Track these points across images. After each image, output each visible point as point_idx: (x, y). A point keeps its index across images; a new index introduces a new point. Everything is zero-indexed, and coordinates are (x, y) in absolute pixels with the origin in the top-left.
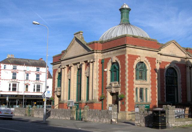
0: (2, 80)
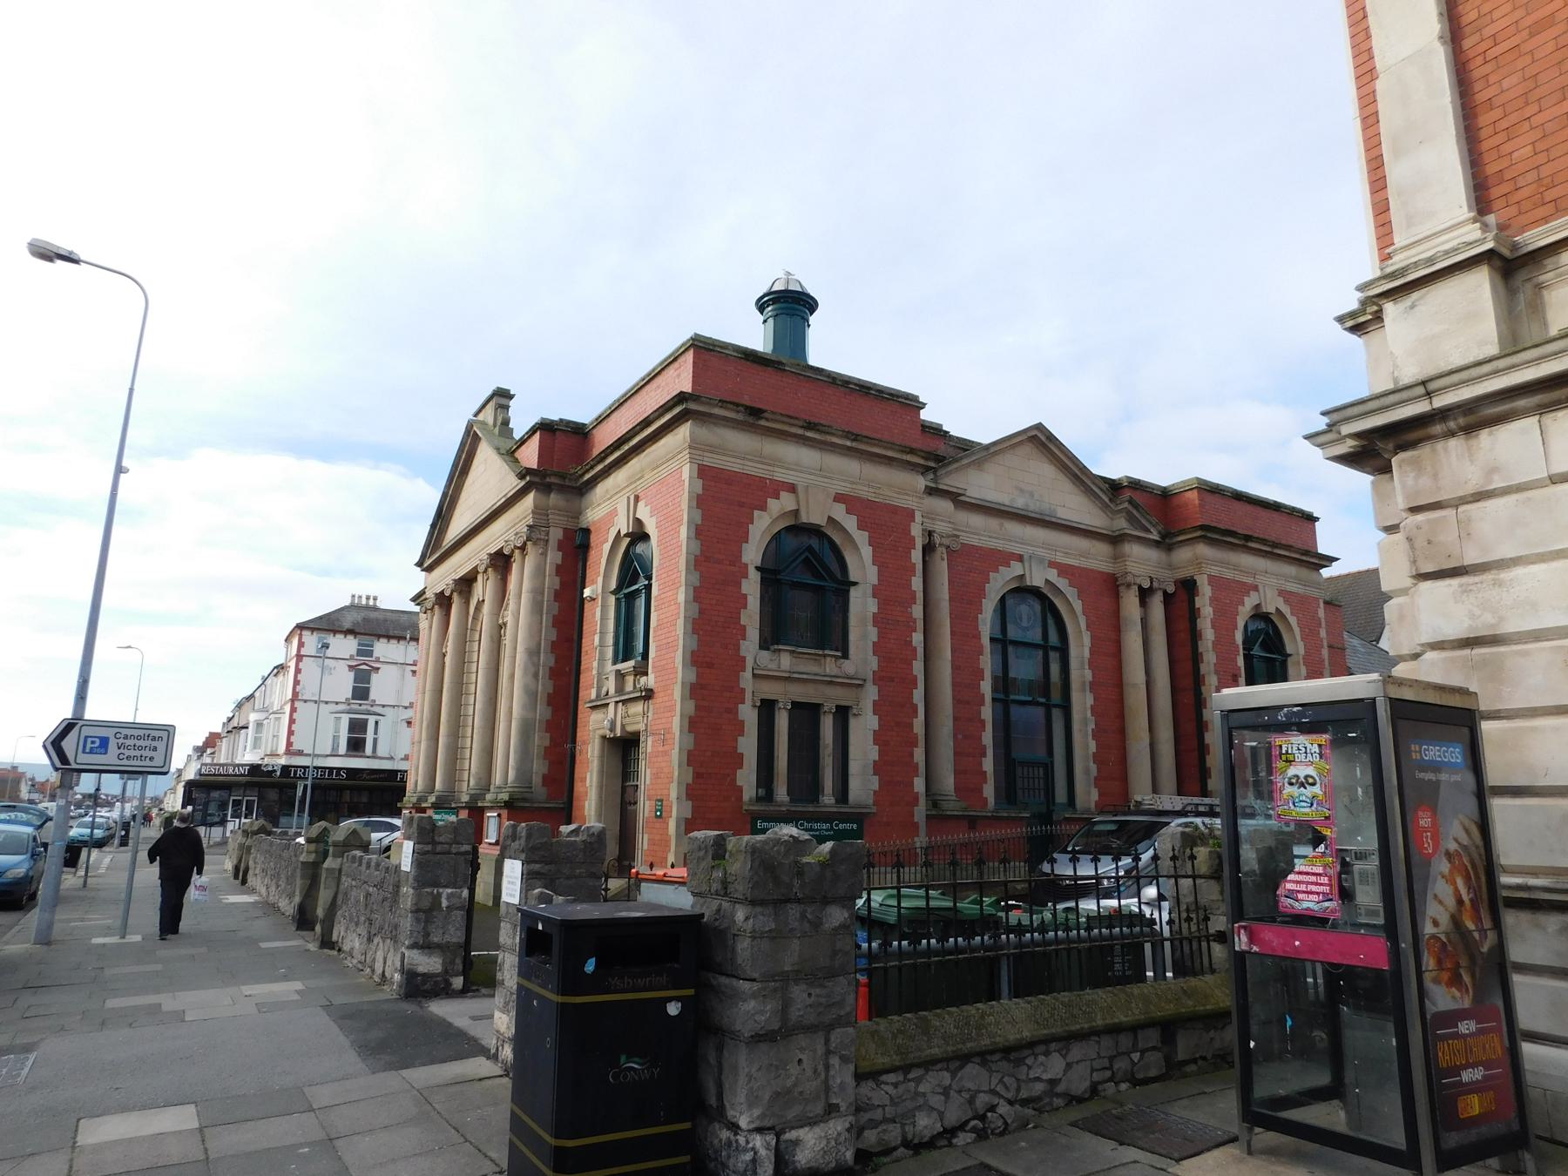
0: (305, 701)
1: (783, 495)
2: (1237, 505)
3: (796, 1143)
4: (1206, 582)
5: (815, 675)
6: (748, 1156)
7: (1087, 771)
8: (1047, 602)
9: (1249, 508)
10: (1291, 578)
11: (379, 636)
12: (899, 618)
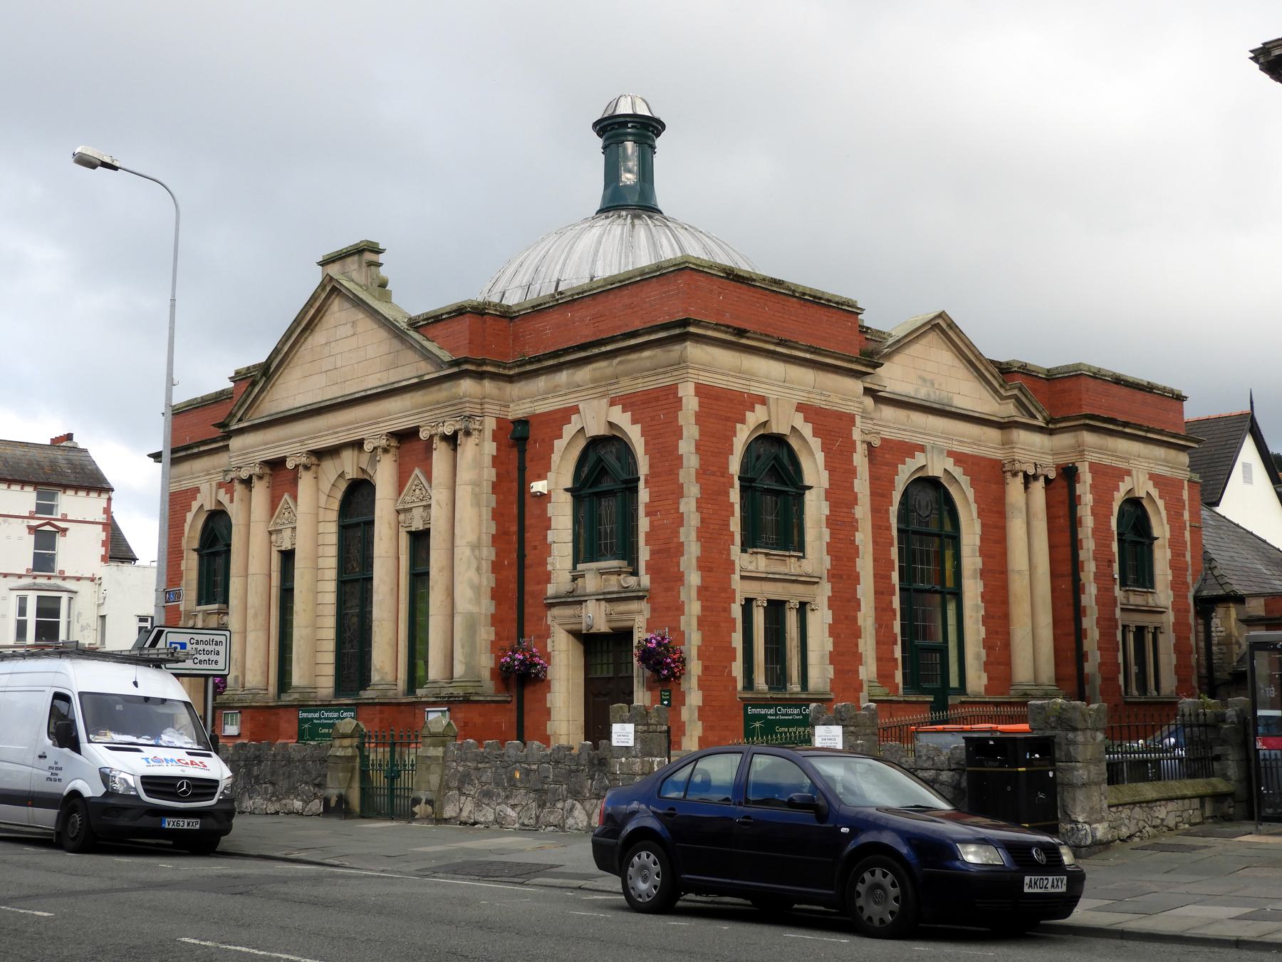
1: (758, 407)
2: (1116, 389)
3: (1096, 829)
4: (1087, 470)
5: (786, 574)
6: (1084, 832)
7: (978, 657)
8: (942, 490)
9: (1126, 391)
10: (1160, 460)
11: (66, 487)
12: (845, 519)
